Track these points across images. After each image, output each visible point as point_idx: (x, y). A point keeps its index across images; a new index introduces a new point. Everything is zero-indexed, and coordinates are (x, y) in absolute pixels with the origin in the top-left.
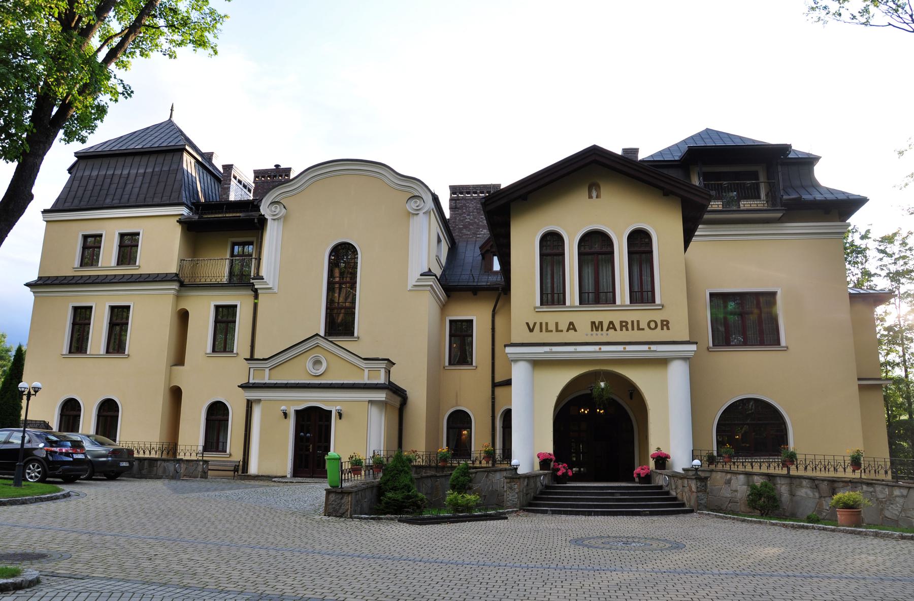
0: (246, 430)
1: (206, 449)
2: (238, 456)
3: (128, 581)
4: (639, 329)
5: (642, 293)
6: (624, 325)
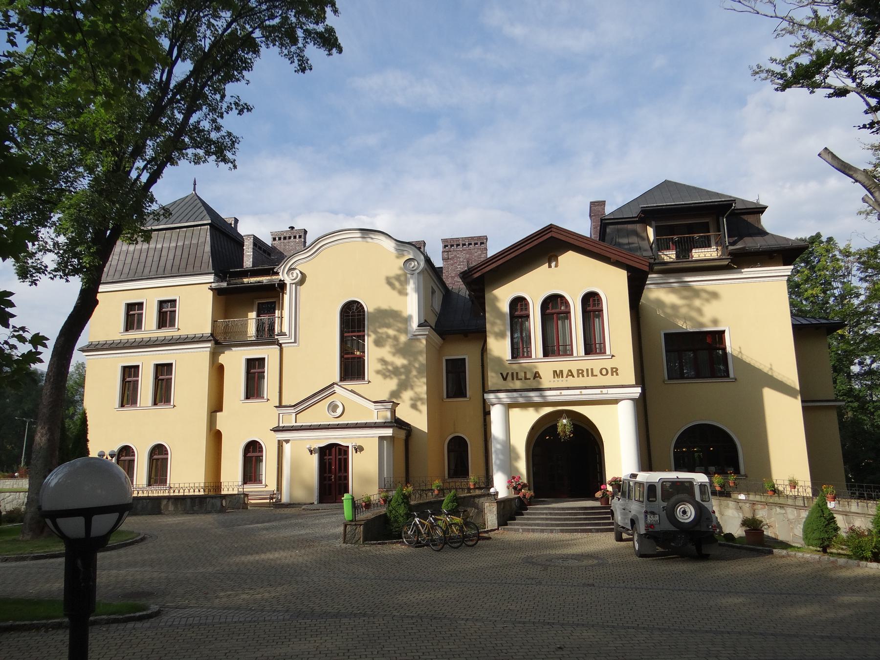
0: (278, 464)
1: (245, 482)
2: (272, 487)
3: (214, 608)
4: (593, 375)
5: (593, 346)
6: (580, 372)
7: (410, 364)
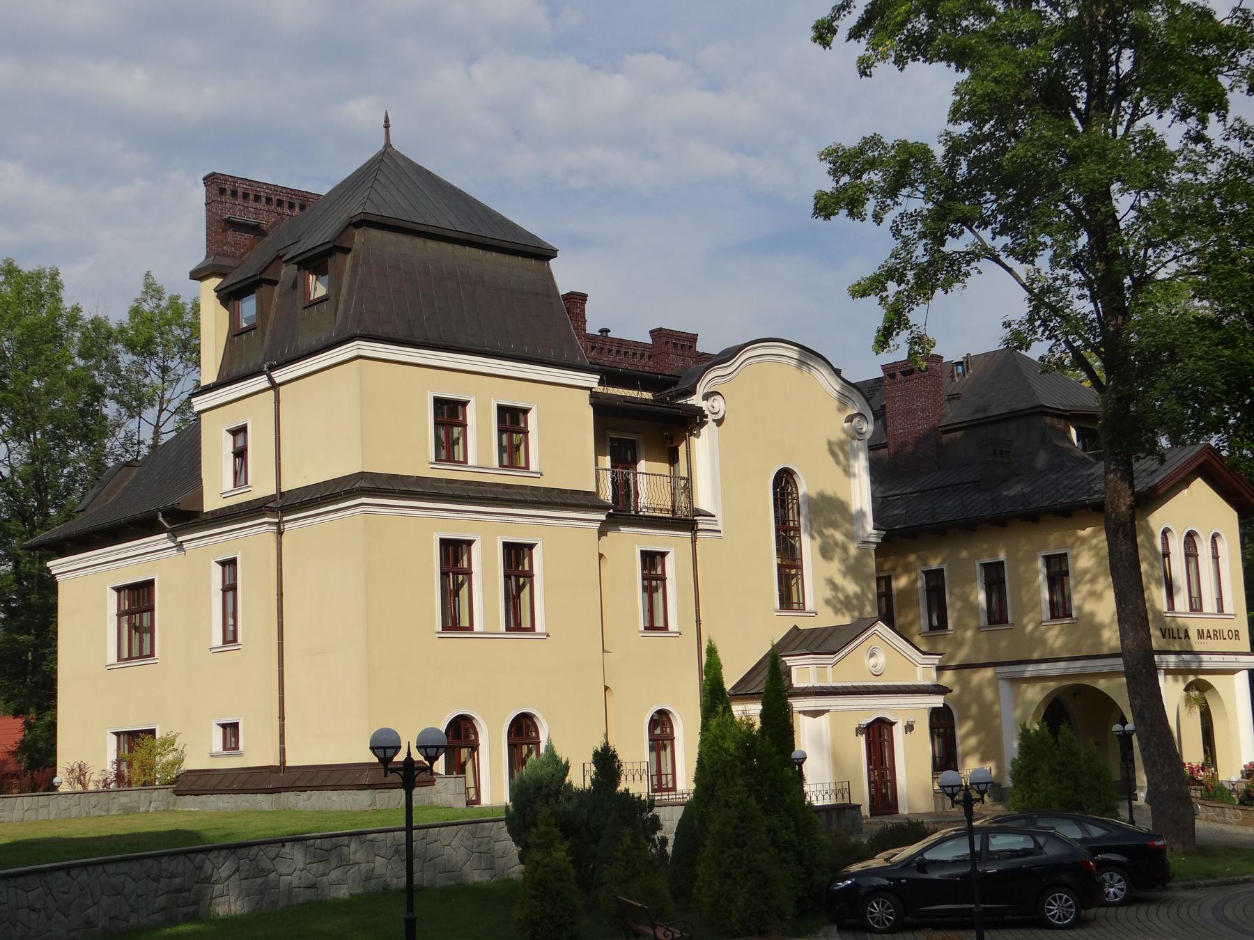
7: (863, 592)
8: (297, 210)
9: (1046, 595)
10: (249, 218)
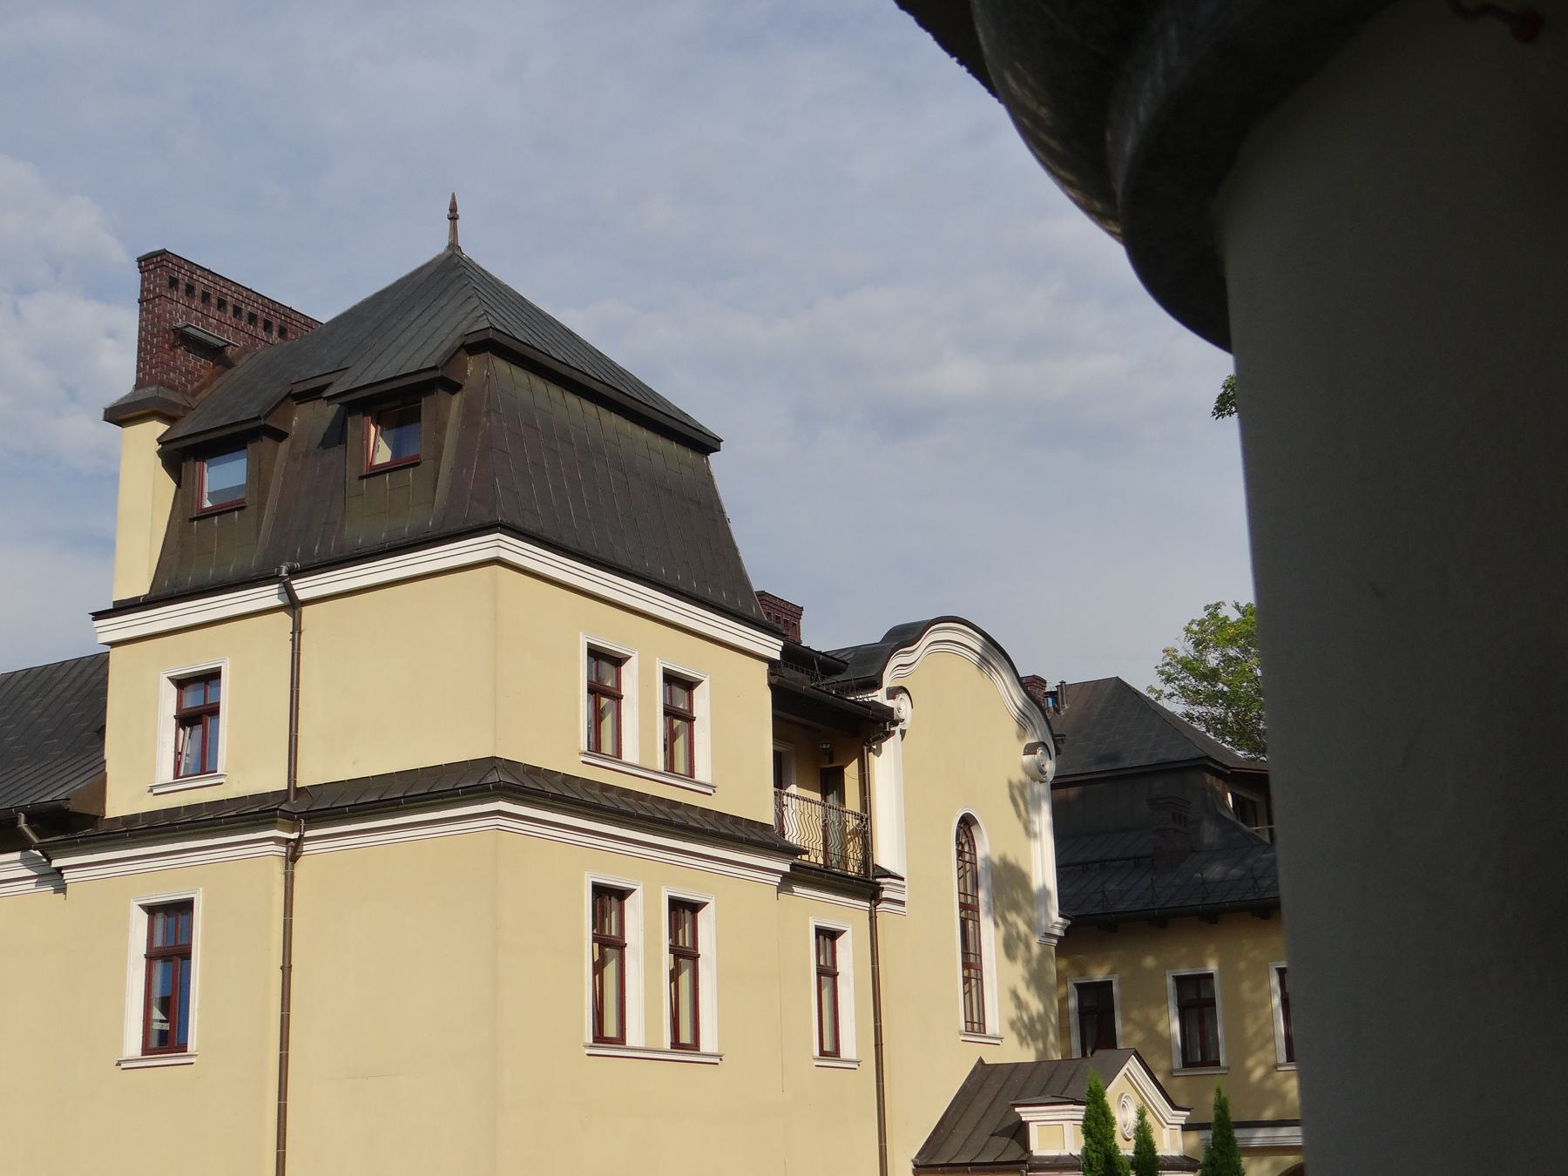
8: (275, 334)
9: (1281, 1028)
10: (214, 336)
